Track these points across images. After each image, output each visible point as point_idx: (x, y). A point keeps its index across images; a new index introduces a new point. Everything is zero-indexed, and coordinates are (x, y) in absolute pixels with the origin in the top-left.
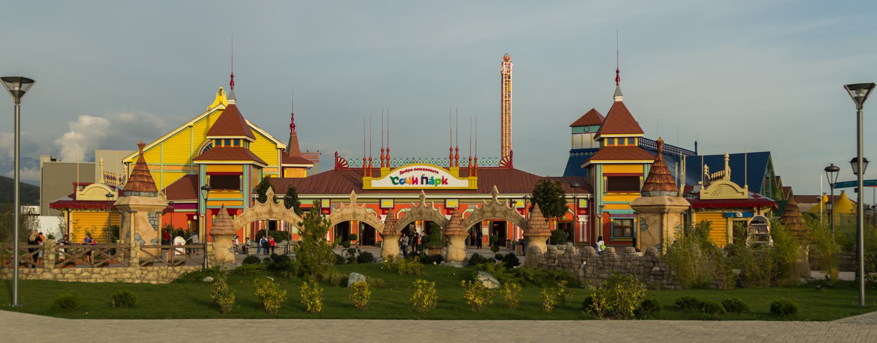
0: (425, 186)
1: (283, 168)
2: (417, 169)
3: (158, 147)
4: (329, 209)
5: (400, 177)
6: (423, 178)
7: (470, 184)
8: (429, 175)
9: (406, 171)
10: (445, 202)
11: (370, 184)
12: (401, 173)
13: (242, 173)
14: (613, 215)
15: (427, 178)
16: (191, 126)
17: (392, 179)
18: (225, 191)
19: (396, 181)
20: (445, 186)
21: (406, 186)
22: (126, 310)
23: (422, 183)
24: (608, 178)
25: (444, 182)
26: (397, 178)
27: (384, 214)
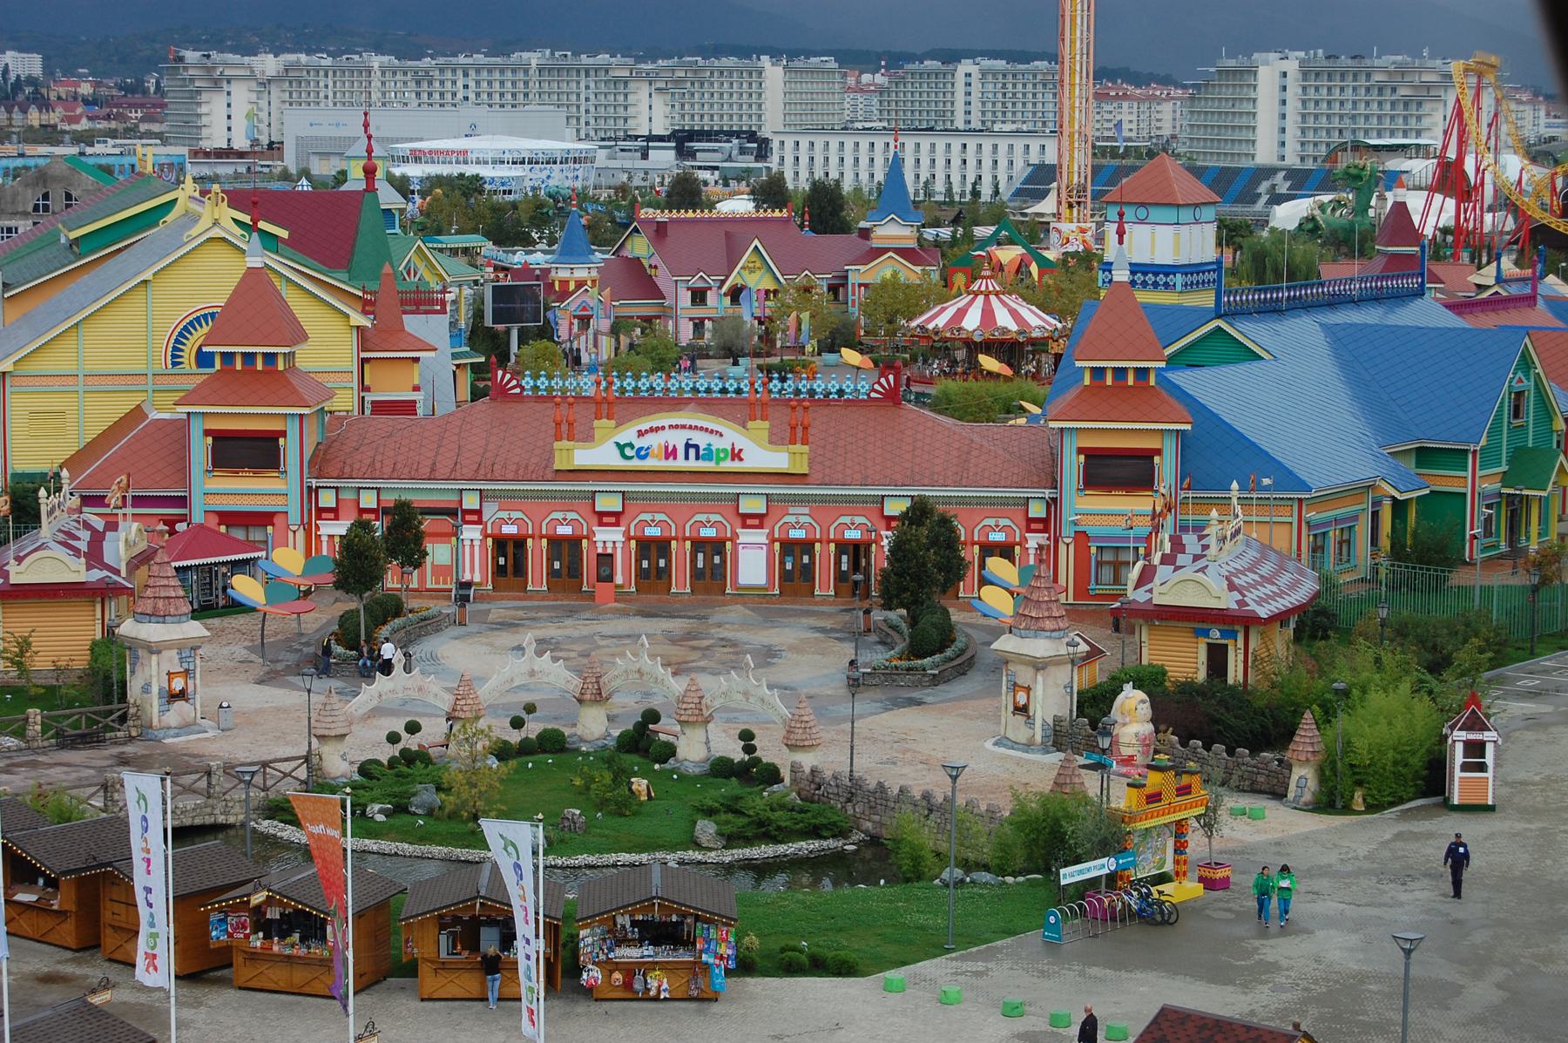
0: (693, 464)
1: (364, 361)
2: (677, 427)
3: (70, 342)
4: (479, 512)
5: (638, 443)
6: (688, 446)
8: (700, 439)
11: (570, 459)
12: (641, 434)
13: (283, 434)
14: (1097, 538)
15: (696, 447)
16: (145, 282)
17: (621, 448)
18: (247, 472)
19: (628, 452)
20: (736, 466)
21: (651, 463)
23: (687, 458)
24: (1087, 457)
25: (736, 455)
26: (631, 446)
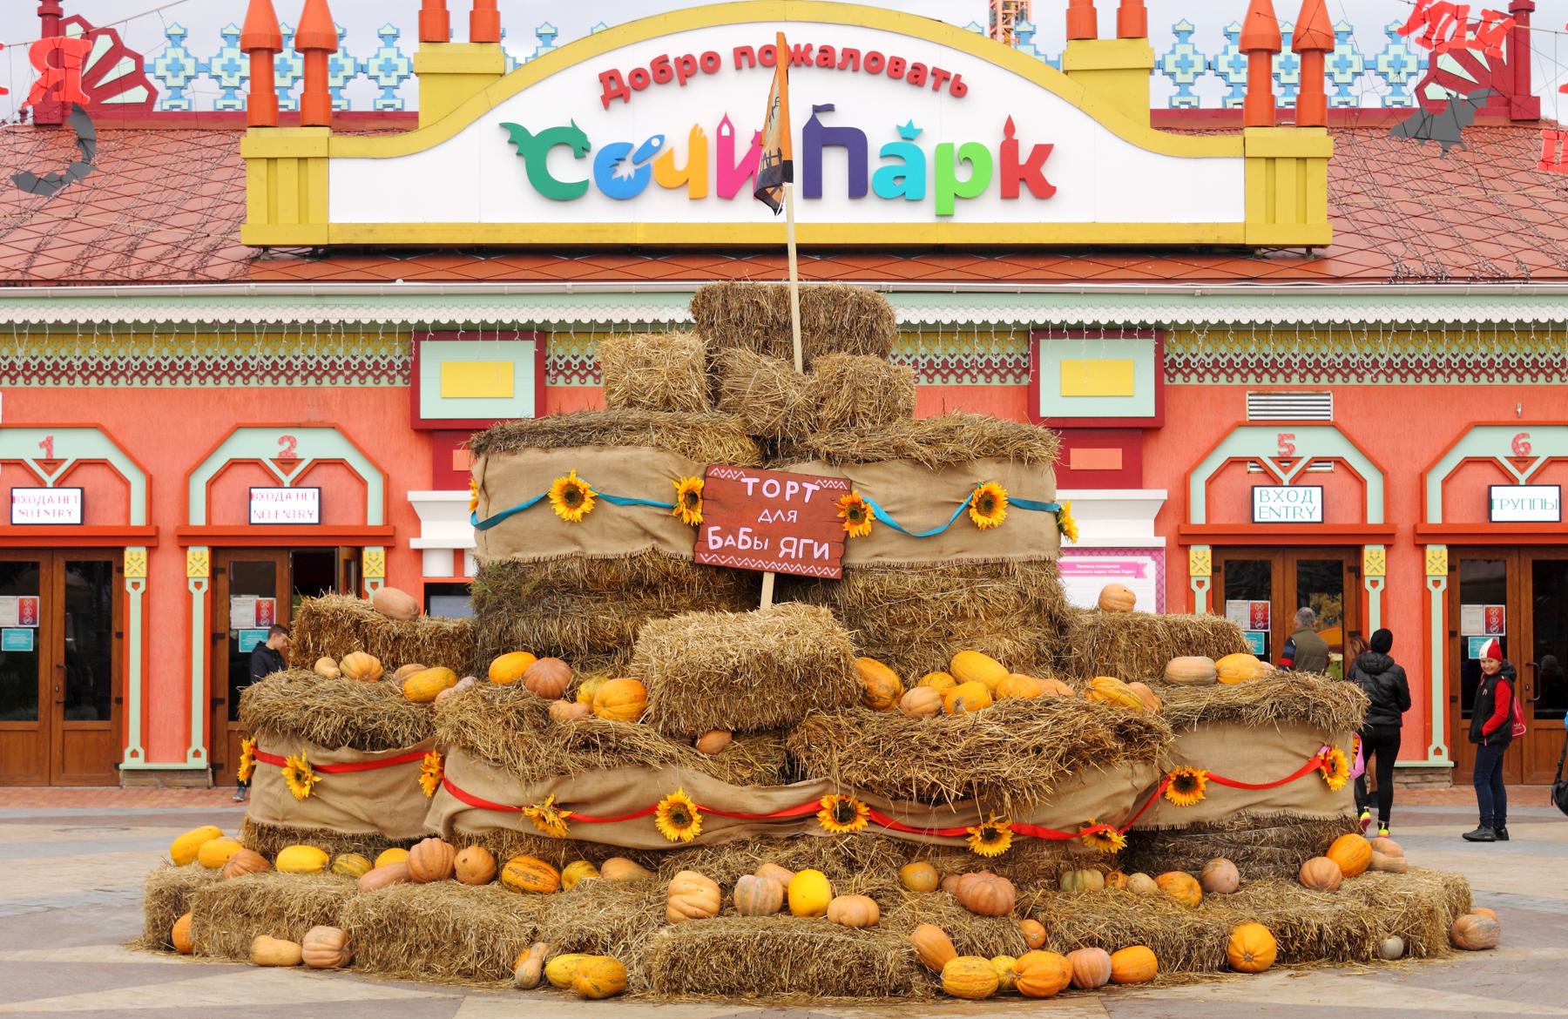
5: (605, 128)
7: (1263, 199)
9: (662, 71)
10: (1031, 368)
11: (311, 200)
12: (615, 89)
15: (853, 141)
17: (531, 148)
19: (564, 168)
20: (1024, 220)
22: (1348, 579)
23: (813, 190)
26: (572, 140)
27: (446, 478)
